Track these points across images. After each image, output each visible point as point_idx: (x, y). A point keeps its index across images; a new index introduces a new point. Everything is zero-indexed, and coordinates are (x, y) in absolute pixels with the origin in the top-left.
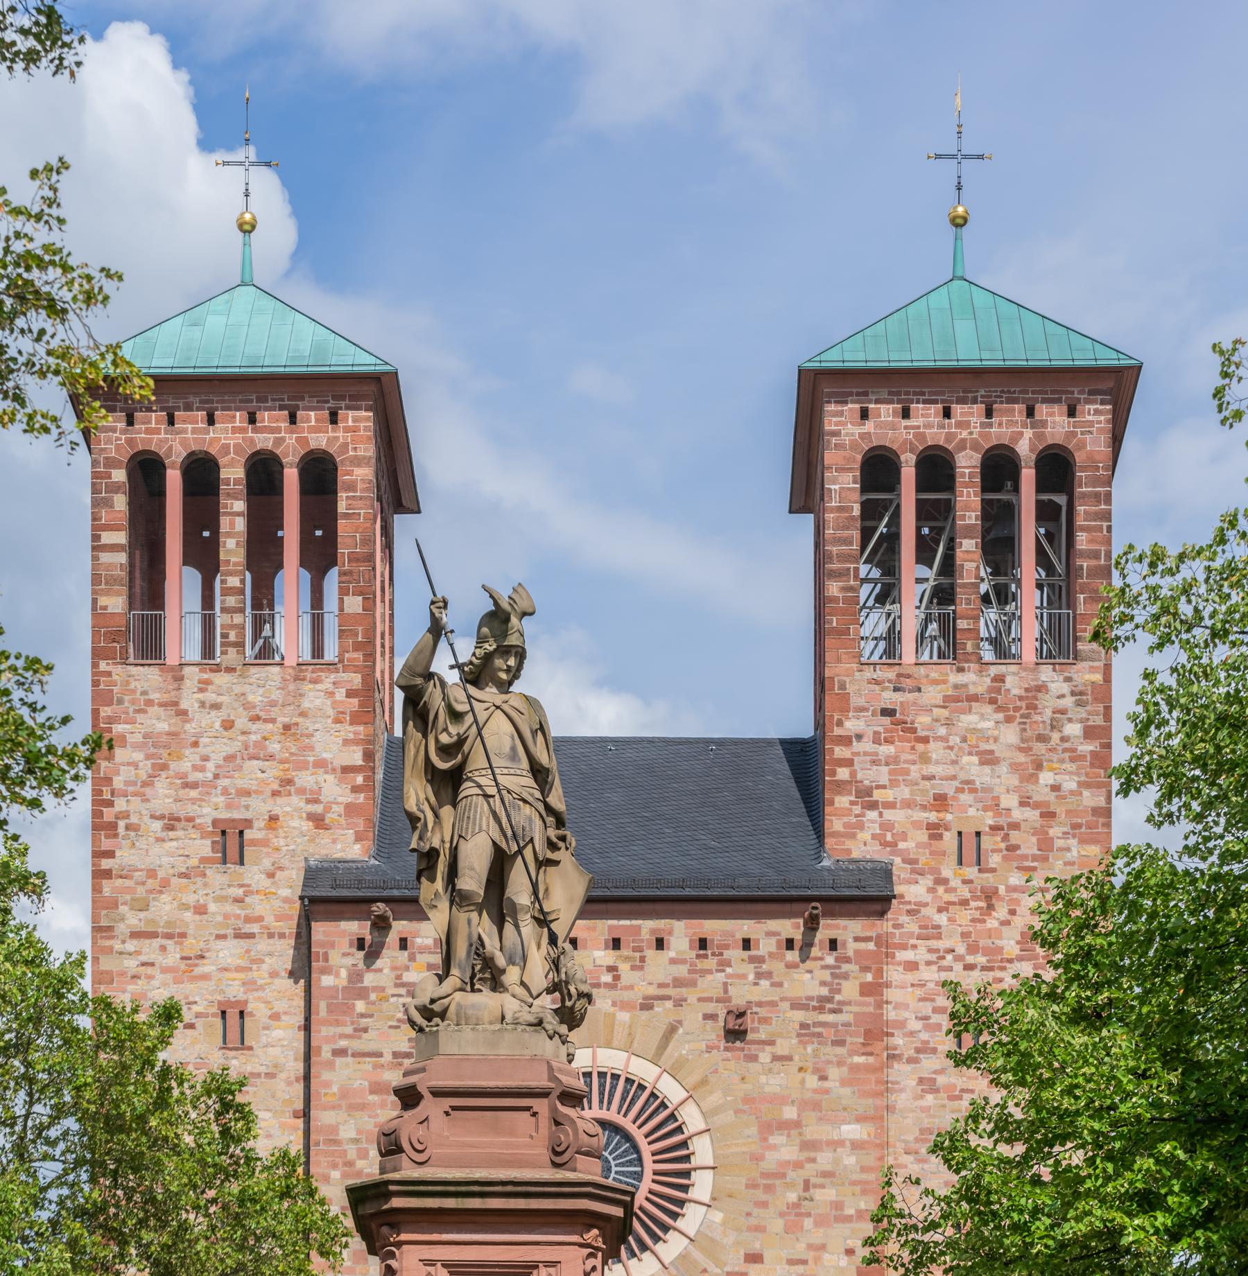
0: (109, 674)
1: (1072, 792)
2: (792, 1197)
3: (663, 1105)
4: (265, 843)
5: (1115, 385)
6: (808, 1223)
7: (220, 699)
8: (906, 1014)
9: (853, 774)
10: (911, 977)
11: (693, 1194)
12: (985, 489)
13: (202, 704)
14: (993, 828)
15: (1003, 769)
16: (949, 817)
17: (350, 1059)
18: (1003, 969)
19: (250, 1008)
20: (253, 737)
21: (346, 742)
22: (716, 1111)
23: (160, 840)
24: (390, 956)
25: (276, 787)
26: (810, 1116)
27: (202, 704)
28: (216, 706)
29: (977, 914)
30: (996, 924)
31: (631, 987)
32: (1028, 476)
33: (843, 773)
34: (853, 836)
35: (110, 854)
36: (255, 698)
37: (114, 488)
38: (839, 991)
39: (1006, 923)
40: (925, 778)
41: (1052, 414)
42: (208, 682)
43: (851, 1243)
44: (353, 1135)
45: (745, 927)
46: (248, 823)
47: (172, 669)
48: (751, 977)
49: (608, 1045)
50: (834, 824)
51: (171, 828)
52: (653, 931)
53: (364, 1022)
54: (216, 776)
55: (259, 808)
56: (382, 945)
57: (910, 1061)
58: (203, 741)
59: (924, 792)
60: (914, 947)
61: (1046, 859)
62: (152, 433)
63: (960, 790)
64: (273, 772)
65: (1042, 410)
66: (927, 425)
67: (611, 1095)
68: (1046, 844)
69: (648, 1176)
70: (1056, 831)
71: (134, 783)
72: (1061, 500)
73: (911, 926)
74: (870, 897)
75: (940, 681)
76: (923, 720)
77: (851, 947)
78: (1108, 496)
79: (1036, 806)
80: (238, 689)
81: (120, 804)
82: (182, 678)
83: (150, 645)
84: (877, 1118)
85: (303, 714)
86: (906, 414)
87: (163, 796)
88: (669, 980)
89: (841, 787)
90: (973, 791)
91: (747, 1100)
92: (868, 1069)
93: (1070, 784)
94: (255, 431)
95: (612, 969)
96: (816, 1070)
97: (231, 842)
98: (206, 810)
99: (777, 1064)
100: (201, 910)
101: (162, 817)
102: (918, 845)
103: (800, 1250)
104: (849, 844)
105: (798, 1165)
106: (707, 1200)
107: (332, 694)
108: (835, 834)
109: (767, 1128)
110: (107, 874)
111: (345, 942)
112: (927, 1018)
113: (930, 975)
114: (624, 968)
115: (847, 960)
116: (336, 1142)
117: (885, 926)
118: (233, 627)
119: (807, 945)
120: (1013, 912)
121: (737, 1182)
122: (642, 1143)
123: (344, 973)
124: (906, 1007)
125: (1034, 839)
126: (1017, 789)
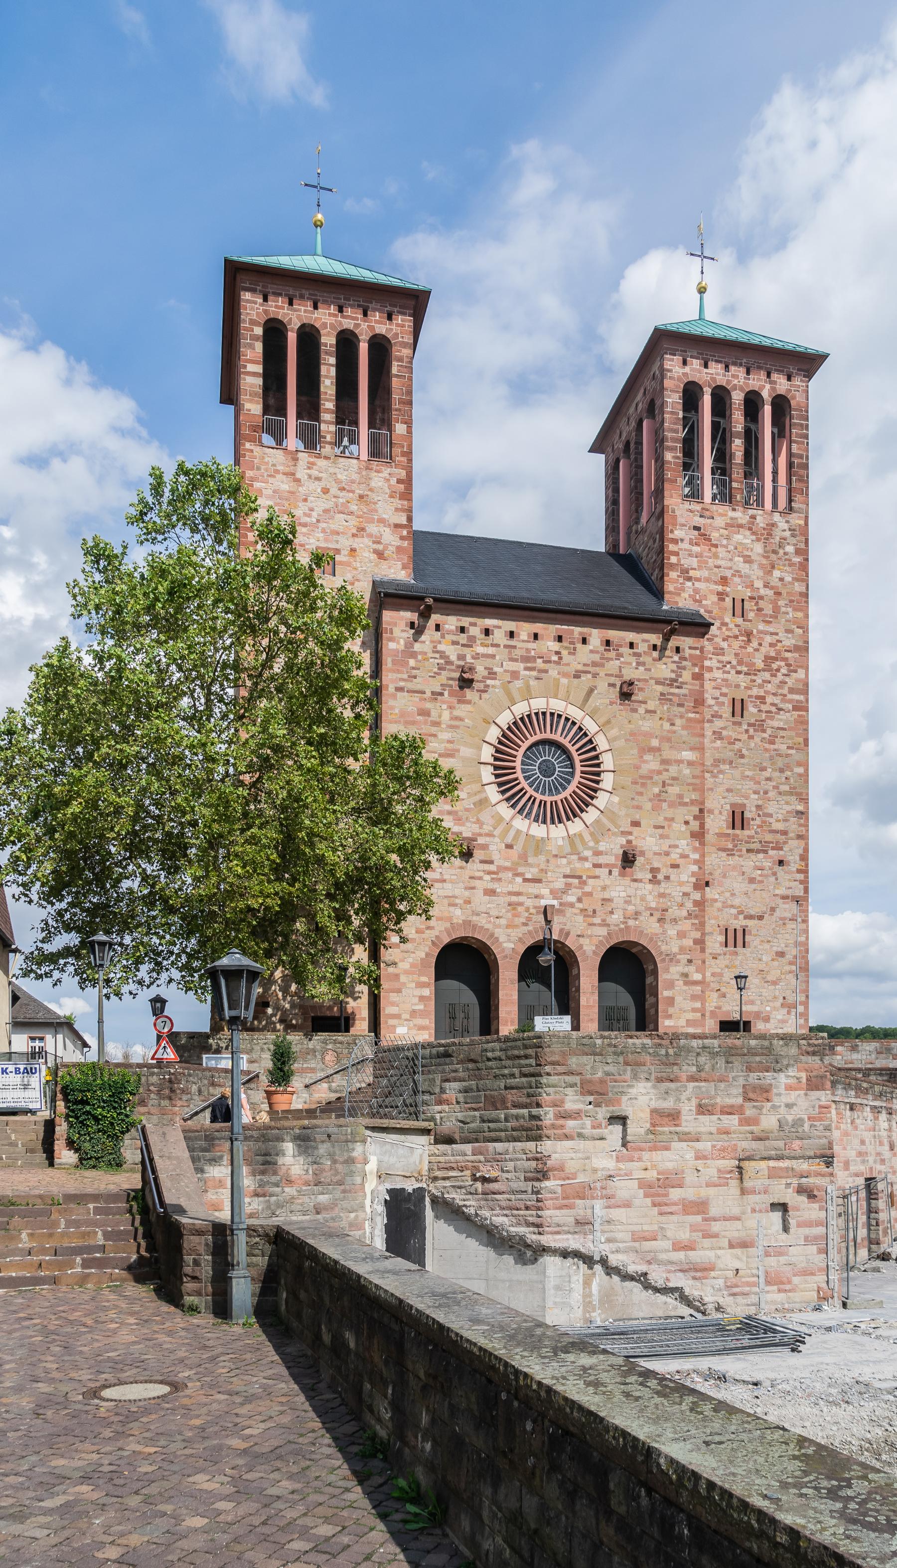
0: (252, 451)
2: (656, 790)
4: (348, 564)
7: (321, 475)
9: (679, 560)
13: (310, 476)
15: (755, 566)
16: (728, 589)
17: (406, 694)
20: (341, 500)
21: (397, 510)
22: (615, 739)
24: (429, 635)
25: (354, 531)
26: (666, 746)
27: (310, 476)
28: (318, 479)
31: (568, 665)
33: (674, 559)
36: (342, 477)
39: (757, 650)
42: (313, 464)
45: (631, 636)
47: (291, 452)
48: (634, 664)
49: (556, 697)
50: (669, 587)
52: (580, 633)
53: (414, 672)
54: (318, 521)
55: (344, 543)
56: (425, 627)
59: (716, 574)
61: (776, 617)
63: (733, 575)
64: (353, 522)
65: (775, 376)
68: (776, 609)
70: (781, 603)
74: (697, 626)
75: (724, 514)
76: (715, 535)
77: (687, 652)
78: (807, 426)
79: (772, 588)
80: (332, 470)
82: (297, 459)
84: (700, 749)
85: (371, 490)
90: (741, 576)
91: (632, 734)
93: (788, 579)
94: (343, 317)
95: (557, 653)
96: (669, 720)
99: (648, 715)
102: (713, 603)
103: (660, 820)
104: (677, 599)
105: (659, 773)
107: (388, 480)
108: (669, 592)
113: (718, 674)
114: (564, 653)
115: (685, 659)
117: (704, 642)
119: (664, 649)
120: (760, 645)
121: (627, 780)
123: (402, 642)
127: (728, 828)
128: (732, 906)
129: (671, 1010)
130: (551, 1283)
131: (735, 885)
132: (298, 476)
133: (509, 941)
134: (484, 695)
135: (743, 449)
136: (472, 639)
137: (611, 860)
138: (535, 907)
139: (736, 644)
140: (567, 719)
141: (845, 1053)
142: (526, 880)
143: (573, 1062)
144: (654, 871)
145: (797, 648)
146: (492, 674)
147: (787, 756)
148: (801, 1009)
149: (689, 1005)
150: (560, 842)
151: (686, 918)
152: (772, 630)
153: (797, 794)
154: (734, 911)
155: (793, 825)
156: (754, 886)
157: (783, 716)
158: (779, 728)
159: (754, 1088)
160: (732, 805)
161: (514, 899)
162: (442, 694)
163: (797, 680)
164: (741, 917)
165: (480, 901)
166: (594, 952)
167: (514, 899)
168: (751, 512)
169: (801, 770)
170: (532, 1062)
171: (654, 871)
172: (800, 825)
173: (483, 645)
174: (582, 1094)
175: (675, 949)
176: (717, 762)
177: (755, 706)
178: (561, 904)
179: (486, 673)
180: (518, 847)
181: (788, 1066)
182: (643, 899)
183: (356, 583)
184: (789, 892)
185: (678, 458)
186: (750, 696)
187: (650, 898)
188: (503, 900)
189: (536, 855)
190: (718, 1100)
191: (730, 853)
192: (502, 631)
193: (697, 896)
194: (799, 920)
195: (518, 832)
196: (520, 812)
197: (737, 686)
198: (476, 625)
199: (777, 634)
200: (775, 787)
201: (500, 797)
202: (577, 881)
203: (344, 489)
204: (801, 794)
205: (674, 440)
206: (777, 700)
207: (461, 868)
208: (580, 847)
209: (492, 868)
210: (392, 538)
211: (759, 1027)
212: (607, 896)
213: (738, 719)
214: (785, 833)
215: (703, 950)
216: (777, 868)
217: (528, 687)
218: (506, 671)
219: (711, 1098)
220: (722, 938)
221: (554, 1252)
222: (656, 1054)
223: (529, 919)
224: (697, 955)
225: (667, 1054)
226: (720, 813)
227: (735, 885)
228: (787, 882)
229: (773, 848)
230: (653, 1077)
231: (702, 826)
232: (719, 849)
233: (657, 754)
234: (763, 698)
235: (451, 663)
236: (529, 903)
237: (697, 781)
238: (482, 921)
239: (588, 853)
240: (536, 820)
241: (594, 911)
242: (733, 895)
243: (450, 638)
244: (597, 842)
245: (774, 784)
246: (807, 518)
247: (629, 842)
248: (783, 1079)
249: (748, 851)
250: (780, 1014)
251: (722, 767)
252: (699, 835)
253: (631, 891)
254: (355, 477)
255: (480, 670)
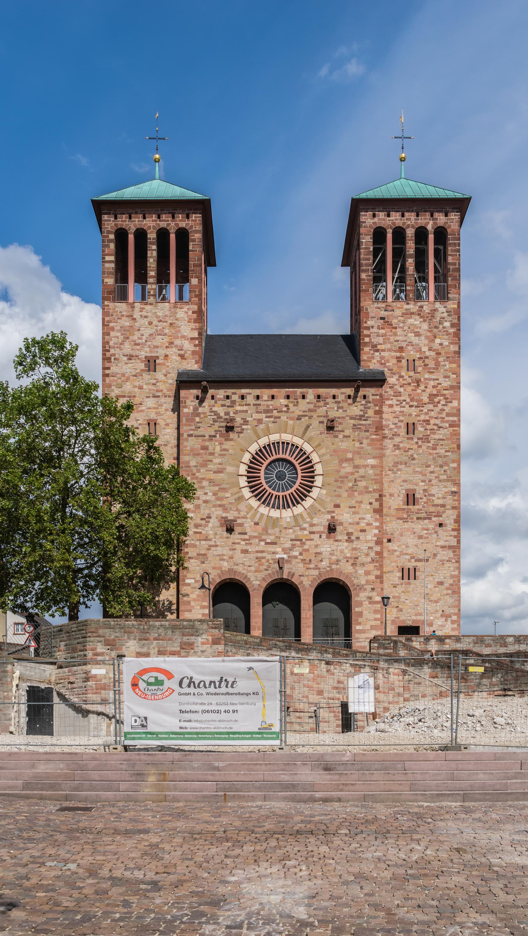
0: (108, 306)
1: (447, 346)
2: (350, 485)
3: (305, 453)
4: (163, 364)
5: (460, 205)
6: (356, 494)
7: (148, 314)
8: (389, 423)
9: (370, 340)
10: (390, 410)
11: (315, 484)
12: (416, 243)
13: (141, 316)
14: (419, 358)
15: (423, 338)
16: (404, 354)
17: (194, 438)
18: (423, 407)
19: (158, 422)
20: (159, 328)
22: (323, 455)
23: (126, 363)
25: (167, 345)
27: (141, 316)
28: (146, 317)
29: (414, 388)
30: (420, 391)
31: (293, 412)
32: (431, 237)
33: (367, 340)
34: (371, 361)
35: (109, 368)
36: (160, 314)
37: (110, 241)
38: (367, 413)
39: (424, 391)
40: (395, 341)
41: (439, 216)
42: (143, 308)
43: (371, 501)
44: (195, 464)
45: (334, 391)
46: (158, 357)
47: (131, 304)
48: (336, 408)
50: (364, 357)
51: (130, 359)
52: (301, 393)
54: (146, 341)
55: (161, 352)
56: (205, 398)
57: (390, 439)
58: (141, 329)
59: (395, 346)
60: (392, 399)
61: (438, 369)
62: (123, 221)
63: (407, 345)
64: (166, 339)
65: (436, 215)
66: (396, 219)
67: (286, 450)
68: (437, 364)
69: (298, 483)
71: (117, 344)
72: (441, 247)
73: (391, 392)
74: (377, 380)
76: (395, 321)
77: (371, 398)
78: (459, 244)
79: (434, 350)
80: (154, 311)
81: (112, 351)
82: (134, 307)
83: (123, 296)
85: (177, 320)
86: (389, 216)
87: (127, 348)
88: (307, 410)
89: (366, 344)
90: (412, 345)
91: (335, 451)
92: (377, 440)
93: (446, 343)
95: (286, 406)
96: (359, 441)
97: (151, 364)
98: (143, 353)
99: (345, 439)
100: (141, 388)
101: (127, 355)
102: (393, 364)
104: (369, 364)
105: (352, 474)
106: (320, 486)
108: (364, 360)
109: (342, 461)
110: (108, 375)
111: (192, 397)
112: (396, 424)
113: (397, 409)
114: (291, 405)
115: (370, 402)
116: (189, 467)
118: (152, 289)
119: (355, 397)
120: (426, 387)
121: (331, 480)
122: (298, 466)
123: (191, 408)
124: (389, 420)
125: (433, 362)
126: (427, 345)
127: (403, 505)
128: (407, 554)
129: (360, 620)
130: (92, 726)
131: (409, 540)
132: (135, 316)
133: (257, 580)
134: (241, 435)
135: (414, 265)
136: (234, 402)
137: (321, 529)
138: (272, 559)
139: (409, 389)
140: (293, 445)
141: (451, 643)
142: (267, 543)
143: (101, 631)
144: (349, 534)
145: (452, 387)
146: (246, 422)
147: (445, 456)
148: (455, 618)
149: (372, 616)
150: (288, 520)
151: (370, 563)
152: (434, 377)
153: (452, 481)
154: (408, 557)
155: (450, 501)
156: (421, 541)
157: (442, 431)
158: (439, 439)
159: (185, 644)
160: (406, 490)
161: (260, 555)
162: (215, 436)
163: (452, 408)
164: (413, 560)
165: (239, 557)
166: (310, 585)
167: (260, 555)
168: (419, 304)
169: (455, 465)
170: (84, 632)
171: (349, 534)
172: (455, 500)
173: (240, 405)
174: (105, 645)
175: (363, 582)
176: (396, 464)
177: (423, 427)
178: (289, 557)
179: (242, 422)
180: (262, 524)
181: (202, 634)
182: (342, 552)
183: (168, 375)
184: (447, 544)
185: (370, 276)
186: (419, 421)
187: (346, 551)
188: (252, 556)
189: (273, 528)
190: (168, 649)
191: (405, 520)
192: (252, 396)
193: (378, 549)
194: (454, 561)
195: (262, 515)
196: (263, 503)
197: (410, 415)
198: (235, 394)
199: (438, 379)
200: (436, 477)
201: (251, 494)
202: (299, 542)
203: (161, 321)
204: (455, 480)
205: (367, 265)
206: (438, 422)
207: (227, 538)
208: (301, 522)
209: (246, 537)
210: (189, 346)
211: (426, 630)
212: (318, 550)
213: (411, 435)
214: (443, 506)
215: (382, 582)
216: (438, 528)
217: (268, 428)
218: (254, 419)
219: (164, 647)
220: (400, 574)
221: (93, 712)
222: (138, 628)
223: (269, 566)
224: (378, 585)
225: (144, 628)
226: (399, 496)
227: (409, 540)
228: (445, 537)
229: (435, 516)
230: (137, 638)
231: (381, 505)
232: (398, 518)
233: (351, 462)
234: (429, 421)
235: (221, 418)
236: (269, 557)
237: (378, 477)
238: (240, 569)
239: (306, 525)
240: (273, 507)
241: (310, 561)
242: (407, 547)
243: (220, 403)
244: (312, 518)
245: (436, 475)
246: (459, 303)
247: (333, 517)
248: (200, 639)
249: (418, 518)
250: (440, 622)
251: (400, 467)
252: (379, 511)
253: (334, 548)
254: (168, 313)
255: (239, 420)
